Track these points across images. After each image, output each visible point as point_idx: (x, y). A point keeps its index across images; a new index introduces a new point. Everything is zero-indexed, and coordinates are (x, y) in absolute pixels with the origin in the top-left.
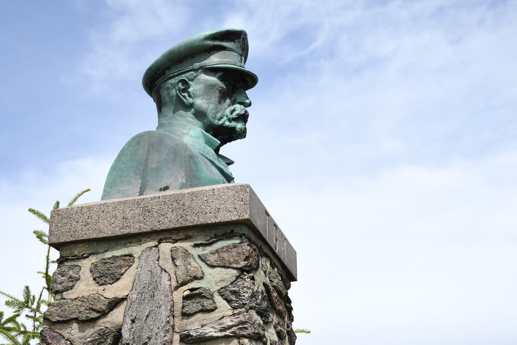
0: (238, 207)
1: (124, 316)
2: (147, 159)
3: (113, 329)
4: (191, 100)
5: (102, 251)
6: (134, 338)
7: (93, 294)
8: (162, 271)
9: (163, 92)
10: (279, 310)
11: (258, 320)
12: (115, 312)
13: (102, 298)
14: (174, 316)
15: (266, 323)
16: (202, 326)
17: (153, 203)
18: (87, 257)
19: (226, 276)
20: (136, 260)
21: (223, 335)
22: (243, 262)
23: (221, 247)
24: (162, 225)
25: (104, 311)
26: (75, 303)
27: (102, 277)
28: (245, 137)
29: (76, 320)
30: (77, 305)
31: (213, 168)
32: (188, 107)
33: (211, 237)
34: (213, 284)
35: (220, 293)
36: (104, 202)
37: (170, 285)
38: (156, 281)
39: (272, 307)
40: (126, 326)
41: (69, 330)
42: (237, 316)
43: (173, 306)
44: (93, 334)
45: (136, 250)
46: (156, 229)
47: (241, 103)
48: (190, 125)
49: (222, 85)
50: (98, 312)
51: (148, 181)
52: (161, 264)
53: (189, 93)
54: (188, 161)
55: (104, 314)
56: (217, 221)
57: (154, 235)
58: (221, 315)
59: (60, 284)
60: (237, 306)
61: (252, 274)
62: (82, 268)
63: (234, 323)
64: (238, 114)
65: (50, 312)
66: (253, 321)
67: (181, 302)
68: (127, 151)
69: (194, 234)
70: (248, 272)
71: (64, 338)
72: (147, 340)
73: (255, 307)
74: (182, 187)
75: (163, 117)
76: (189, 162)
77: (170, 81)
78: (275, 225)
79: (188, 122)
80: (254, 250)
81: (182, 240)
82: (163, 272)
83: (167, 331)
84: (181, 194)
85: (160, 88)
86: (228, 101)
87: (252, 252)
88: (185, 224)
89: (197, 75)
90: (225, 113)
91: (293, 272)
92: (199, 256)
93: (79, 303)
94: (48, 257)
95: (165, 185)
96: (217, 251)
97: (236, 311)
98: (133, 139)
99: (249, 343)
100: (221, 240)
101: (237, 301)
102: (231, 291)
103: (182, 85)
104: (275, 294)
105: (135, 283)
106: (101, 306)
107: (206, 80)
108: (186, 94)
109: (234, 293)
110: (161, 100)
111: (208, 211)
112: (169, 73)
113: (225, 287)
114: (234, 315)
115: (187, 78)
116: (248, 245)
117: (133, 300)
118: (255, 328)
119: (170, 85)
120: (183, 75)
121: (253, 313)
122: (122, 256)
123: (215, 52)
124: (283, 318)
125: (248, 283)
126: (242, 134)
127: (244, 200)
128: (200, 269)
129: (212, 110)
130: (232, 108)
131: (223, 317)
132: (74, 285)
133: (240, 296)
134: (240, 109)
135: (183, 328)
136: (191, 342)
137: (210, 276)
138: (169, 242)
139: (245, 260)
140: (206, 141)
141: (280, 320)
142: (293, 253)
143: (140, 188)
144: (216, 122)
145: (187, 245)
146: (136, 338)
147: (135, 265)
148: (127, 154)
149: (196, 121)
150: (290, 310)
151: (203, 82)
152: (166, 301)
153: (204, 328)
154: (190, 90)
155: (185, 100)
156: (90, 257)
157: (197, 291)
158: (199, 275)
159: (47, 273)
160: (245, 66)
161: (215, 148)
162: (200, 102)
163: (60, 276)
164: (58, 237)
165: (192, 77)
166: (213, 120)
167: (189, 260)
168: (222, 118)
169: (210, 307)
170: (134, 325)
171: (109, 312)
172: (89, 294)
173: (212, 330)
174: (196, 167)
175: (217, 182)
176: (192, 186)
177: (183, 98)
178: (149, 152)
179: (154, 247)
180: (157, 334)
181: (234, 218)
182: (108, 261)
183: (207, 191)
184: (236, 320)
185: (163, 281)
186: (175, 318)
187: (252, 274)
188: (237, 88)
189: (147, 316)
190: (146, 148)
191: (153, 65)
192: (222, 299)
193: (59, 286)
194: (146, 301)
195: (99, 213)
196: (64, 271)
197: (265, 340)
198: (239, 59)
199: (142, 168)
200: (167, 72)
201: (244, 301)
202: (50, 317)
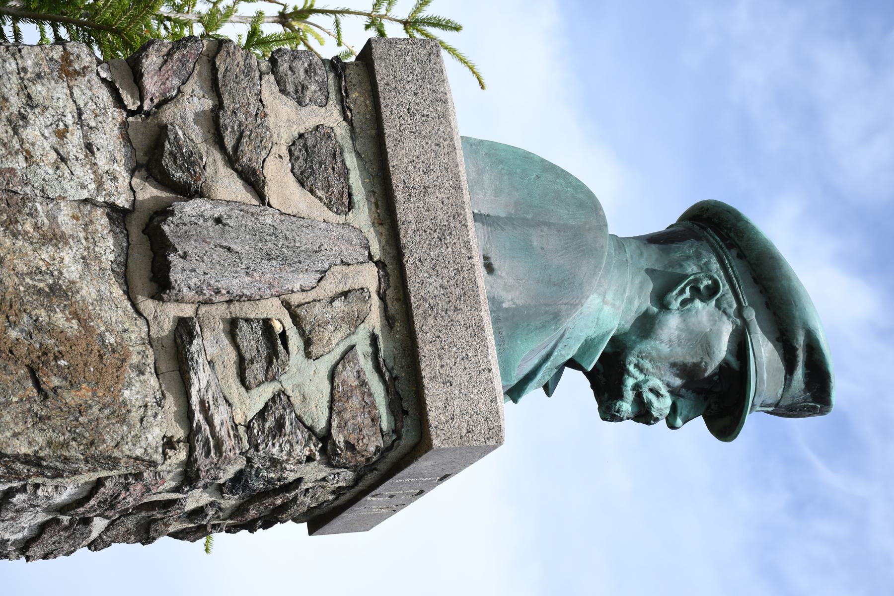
0: (457, 421)
1: (228, 202)
2: (548, 225)
3: (203, 180)
4: (675, 305)
5: (358, 148)
6: (184, 224)
7: (271, 136)
8: (321, 272)
9: (691, 247)
10: (248, 510)
11: (230, 472)
12: (235, 183)
13: (264, 154)
14: (229, 302)
15: (220, 489)
16: (211, 363)
17: (458, 246)
18: (345, 118)
19: (313, 405)
20: (341, 219)
21: (193, 407)
22: (342, 440)
23: (372, 390)
24: (413, 267)
25: (238, 160)
26: (253, 100)
27: (306, 150)
28: (604, 419)
29: (219, 106)
30: (249, 104)
31: (536, 361)
32: (661, 301)
33: (393, 369)
34: (297, 380)
35: (279, 395)
36: (458, 143)
37: (293, 292)
38: (300, 262)
39: (254, 496)
40: (209, 206)
41: (199, 92)
42: (232, 433)
43: (250, 299)
44: (192, 140)
45: (362, 216)
46: (406, 256)
47: (674, 408)
48: (624, 305)
49: (711, 368)
50: (236, 148)
51: (503, 230)
52: (334, 269)
53: (690, 300)
54: (547, 313)
55: (232, 160)
56: (426, 381)
57: (393, 252)
58: (234, 399)
59: (290, 68)
60: (252, 432)
61: (318, 458)
62: (324, 109)
63: (218, 429)
64: (650, 403)
65: (234, 53)
66: (223, 467)
67: (258, 316)
68: (563, 182)
69: (397, 333)
70: (323, 451)
71: (184, 83)
72: (180, 252)
73: (252, 467)
74: (495, 302)
75: (638, 247)
76: (546, 312)
77: (714, 260)
78: (421, 493)
79: (630, 301)
80: (368, 459)
81: (385, 309)
82: (319, 276)
83: (199, 292)
84: (478, 303)
85: (698, 238)
86: (677, 382)
87: (363, 456)
88: (417, 313)
89: (729, 316)
90: (651, 376)
91: (326, 527)
92: (352, 347)
93: (253, 110)
94: (348, 12)
95: (496, 266)
96: (364, 383)
97: (242, 430)
98: (590, 195)
99: (178, 462)
100: (387, 390)
101: (263, 432)
102: (282, 417)
103: (707, 287)
104: (279, 502)
105: (294, 219)
106: (247, 155)
107: (719, 335)
108: (687, 294)
109: (280, 424)
110: (673, 242)
111: (446, 360)
112: (731, 257)
113: (290, 404)
114: (235, 427)
115: (723, 295)
116: (377, 447)
117: (261, 218)
118: (208, 471)
119: (705, 260)
120: (727, 287)
121: (241, 464)
122: (349, 188)
123: (782, 351)
124: (231, 517)
125: (301, 451)
126: (609, 413)
127: (470, 435)
128: (327, 350)
129: (657, 350)
130: (664, 391)
131: (230, 405)
132: (287, 94)
133: (274, 437)
134: (662, 407)
135: (207, 322)
136: (179, 341)
137: (312, 373)
138: (380, 283)
139: (347, 442)
140: (592, 340)
141: (228, 512)
142: (366, 525)
143: (488, 215)
144: (632, 359)
145: (375, 320)
146: (185, 228)
147: (331, 216)
148: (557, 183)
149: (632, 317)
150: (251, 527)
151: (714, 328)
152: (260, 286)
153: (207, 367)
154: (698, 303)
155: (675, 293)
156: (345, 123)
157: (281, 348)
158: (315, 350)
159: (311, 11)
160: (754, 413)
161: (578, 360)
162: (672, 324)
163: (306, 65)
164: (384, 56)
165: (725, 306)
166: (635, 352)
167: (345, 326)
168: (641, 370)
169: (249, 377)
170: (210, 223)
171: (236, 170)
172: (271, 126)
173: (204, 384)
174: (537, 328)
175: (505, 373)
176: (496, 321)
177: (679, 288)
178: (563, 228)
179: (370, 253)
180: (193, 270)
181: (433, 417)
182: (339, 160)
183: (487, 356)
184: (223, 433)
185: (301, 276)
186: (226, 305)
187: (318, 458)
188: (705, 399)
189: (229, 249)
190: (572, 222)
191: (747, 222)
192: (267, 400)
193: (286, 65)
194: (260, 245)
195: (434, 137)
196: (315, 74)
197: (186, 489)
198: (769, 402)
199: (529, 216)
200: (734, 252)
201: (263, 446)
202: (223, 53)
